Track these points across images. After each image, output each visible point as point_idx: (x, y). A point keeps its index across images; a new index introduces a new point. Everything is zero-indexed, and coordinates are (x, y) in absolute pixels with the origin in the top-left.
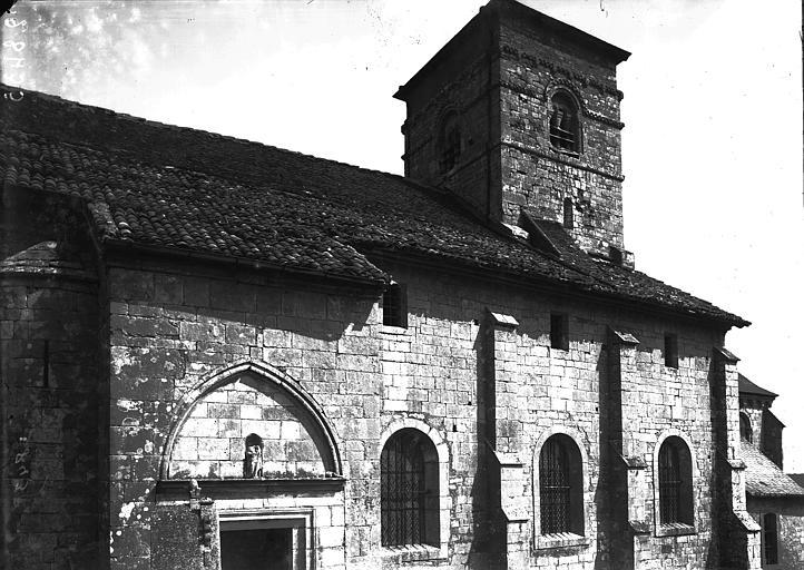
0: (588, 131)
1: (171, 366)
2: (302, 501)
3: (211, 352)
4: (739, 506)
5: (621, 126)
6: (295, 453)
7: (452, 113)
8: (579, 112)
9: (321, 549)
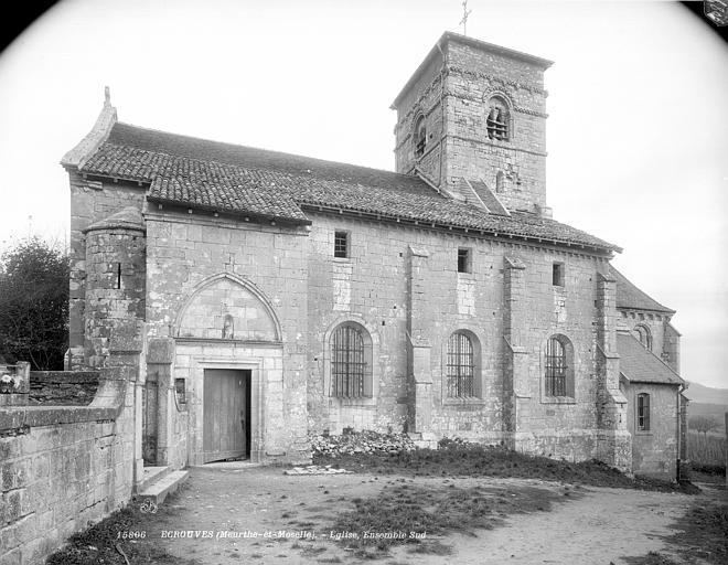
0: (518, 123)
1: (179, 274)
2: (258, 352)
3: (202, 267)
4: (612, 385)
5: (545, 116)
6: (252, 325)
7: (422, 117)
8: (512, 108)
9: (268, 382)
